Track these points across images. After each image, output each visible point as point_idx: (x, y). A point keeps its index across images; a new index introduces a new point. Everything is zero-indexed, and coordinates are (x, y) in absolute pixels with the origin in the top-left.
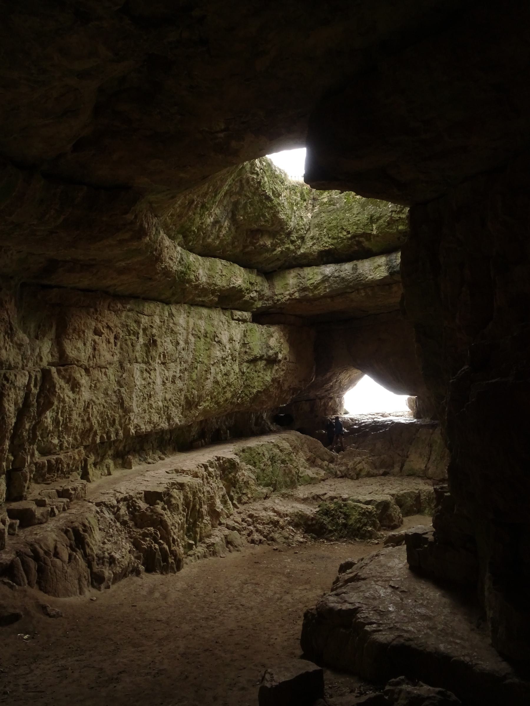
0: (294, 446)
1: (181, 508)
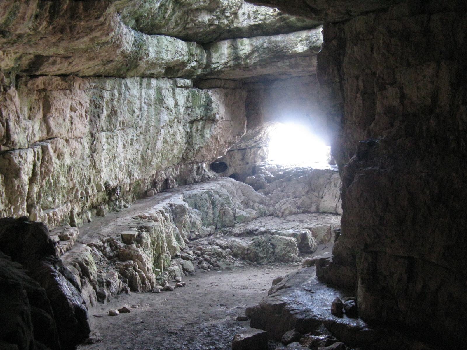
1: (149, 246)
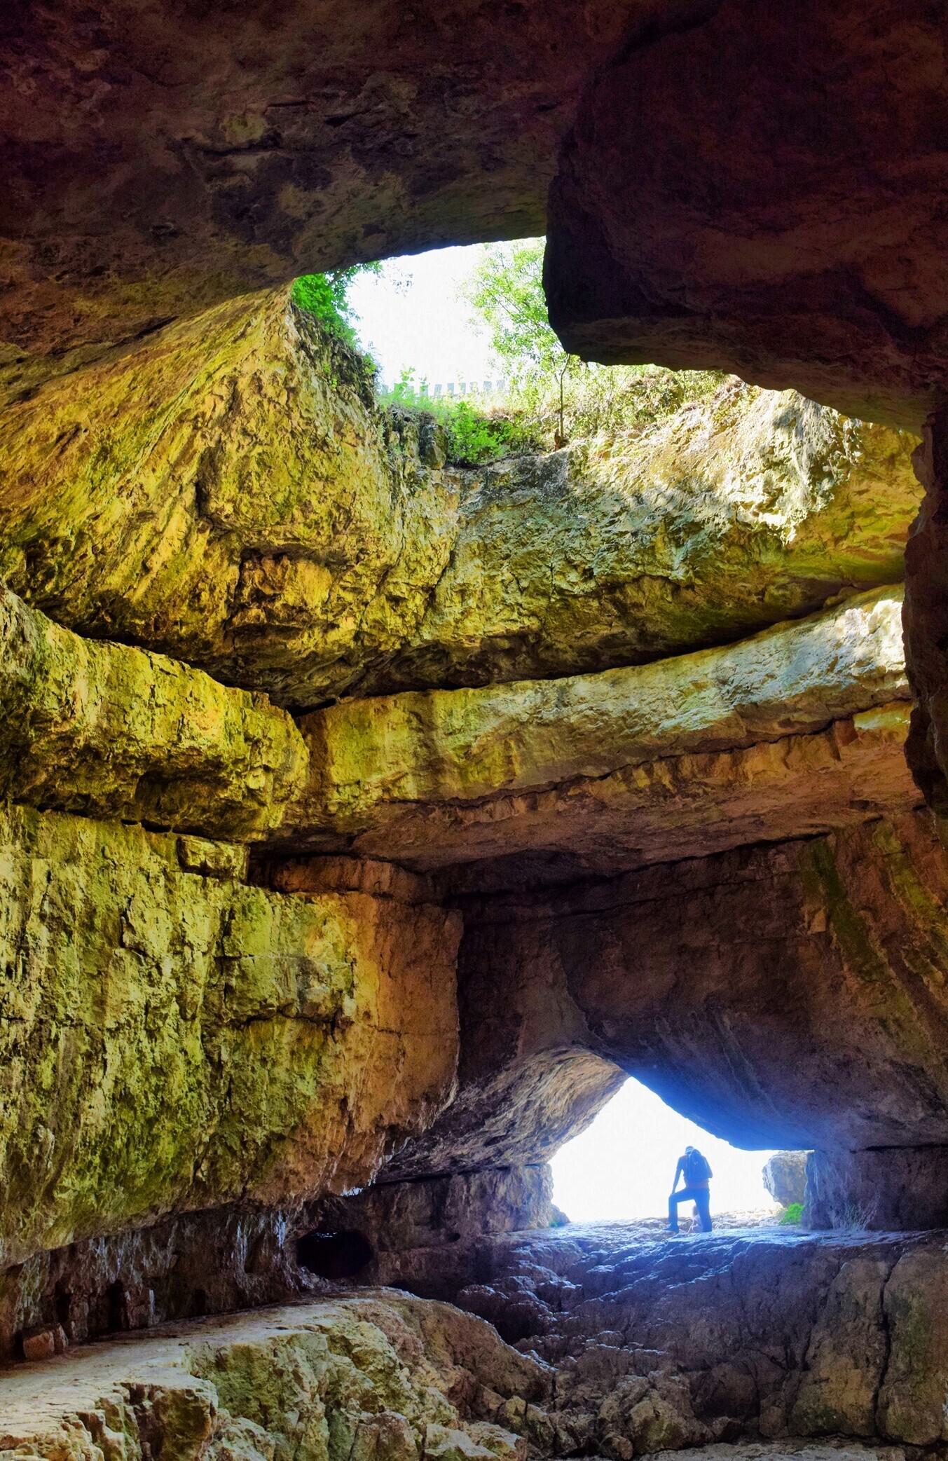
0: (400, 1341)
